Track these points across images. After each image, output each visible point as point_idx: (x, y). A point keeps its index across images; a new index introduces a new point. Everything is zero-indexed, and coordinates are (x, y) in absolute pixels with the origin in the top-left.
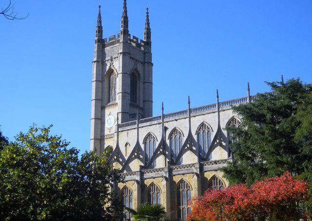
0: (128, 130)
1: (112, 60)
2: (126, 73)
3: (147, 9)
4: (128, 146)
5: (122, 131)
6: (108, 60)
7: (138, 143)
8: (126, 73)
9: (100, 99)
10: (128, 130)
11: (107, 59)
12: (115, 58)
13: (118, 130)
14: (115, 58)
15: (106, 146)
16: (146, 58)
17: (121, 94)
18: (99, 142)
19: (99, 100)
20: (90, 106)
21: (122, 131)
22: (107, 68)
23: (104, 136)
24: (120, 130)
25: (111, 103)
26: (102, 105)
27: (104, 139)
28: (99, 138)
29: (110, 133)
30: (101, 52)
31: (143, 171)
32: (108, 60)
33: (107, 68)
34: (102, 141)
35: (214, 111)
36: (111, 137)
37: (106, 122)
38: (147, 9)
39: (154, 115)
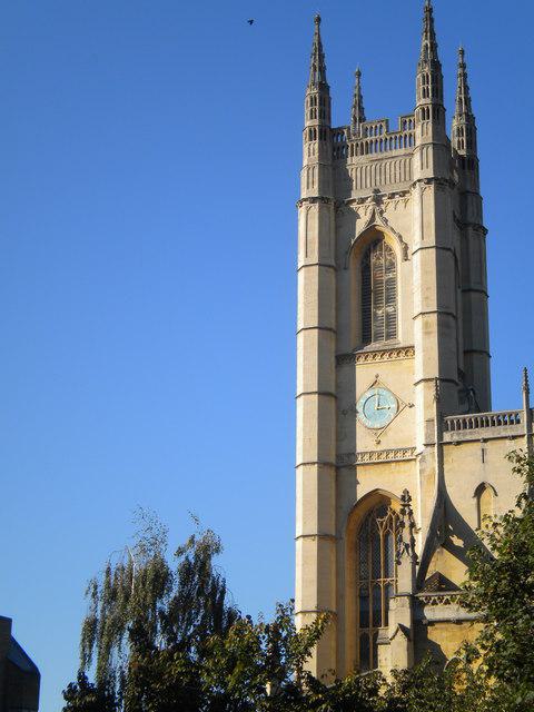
0: (485, 440)
1: (378, 200)
2: (449, 249)
3: (462, 52)
4: (487, 495)
5: (458, 443)
6: (362, 201)
7: (443, 501)
8: (449, 249)
9: (333, 327)
10: (485, 440)
11: (355, 195)
12: (392, 196)
13: (440, 437)
14: (392, 196)
15: (361, 492)
16: (470, 210)
17: (434, 318)
18: (332, 472)
19: (330, 329)
20: (404, 333)
21: (458, 443)
22: (360, 226)
23: (352, 454)
24: (447, 437)
25: (373, 346)
26: (336, 351)
27: (353, 468)
28: (333, 459)
29: (379, 448)
30: (330, 169)
31: (422, 596)
32: (362, 201)
33: (360, 226)
34: (344, 471)
35: (519, 433)
36: (401, 457)
37: (359, 408)
38: (462, 52)
39: (499, 405)
